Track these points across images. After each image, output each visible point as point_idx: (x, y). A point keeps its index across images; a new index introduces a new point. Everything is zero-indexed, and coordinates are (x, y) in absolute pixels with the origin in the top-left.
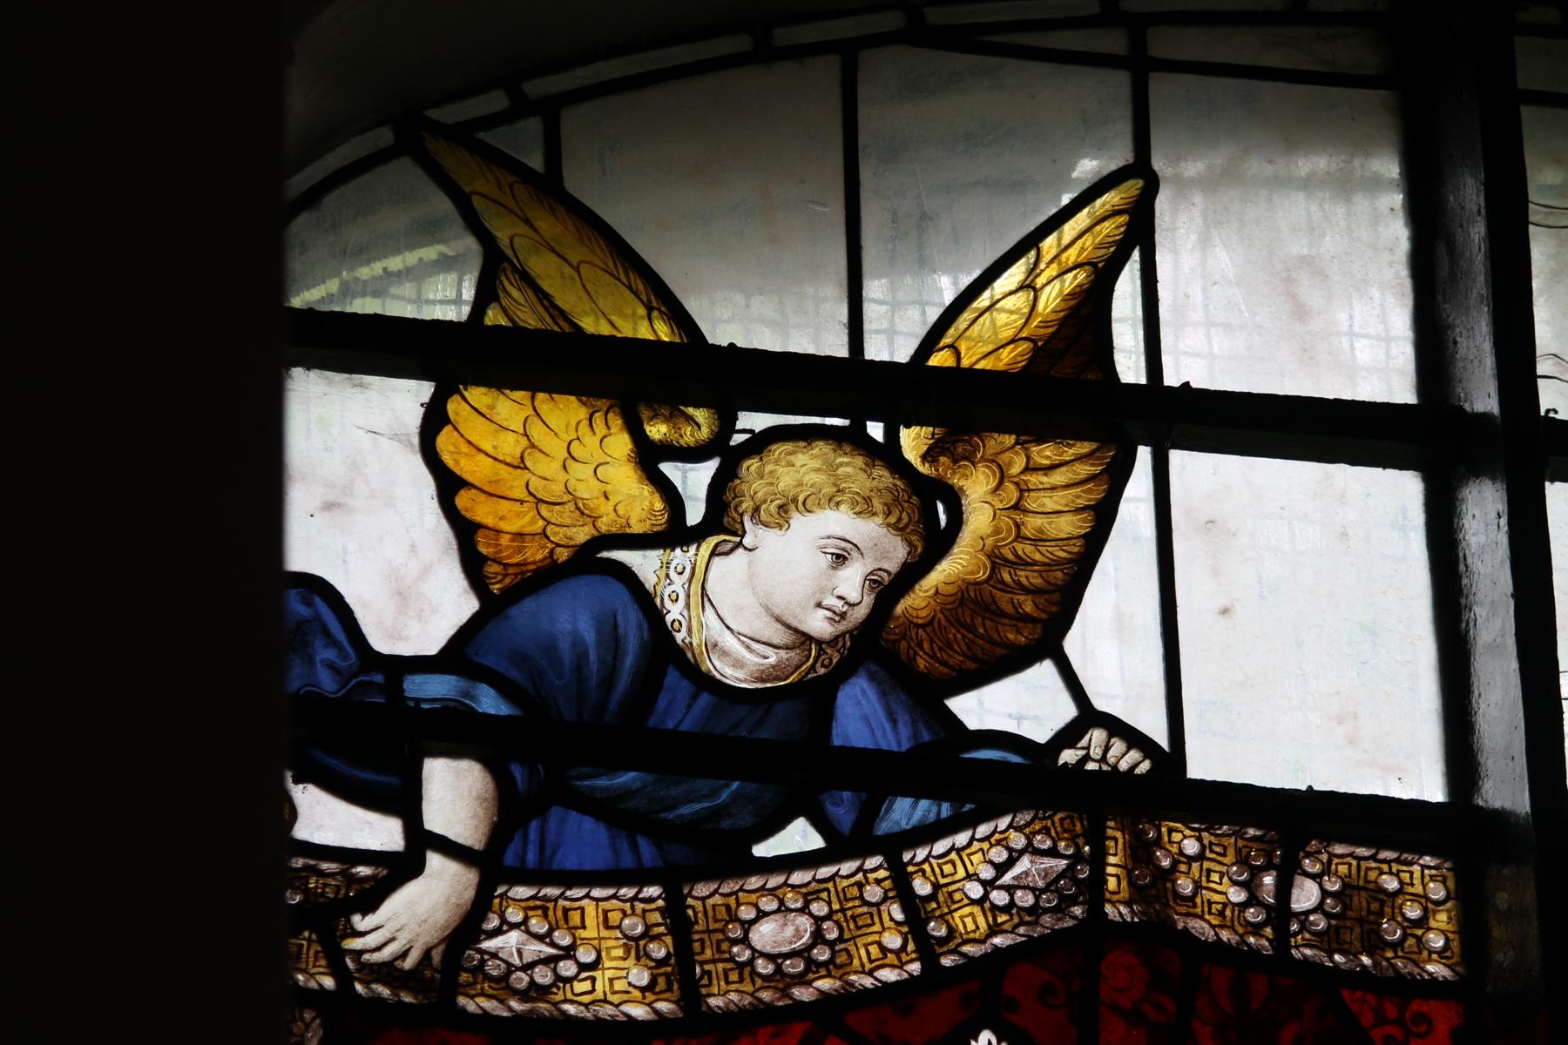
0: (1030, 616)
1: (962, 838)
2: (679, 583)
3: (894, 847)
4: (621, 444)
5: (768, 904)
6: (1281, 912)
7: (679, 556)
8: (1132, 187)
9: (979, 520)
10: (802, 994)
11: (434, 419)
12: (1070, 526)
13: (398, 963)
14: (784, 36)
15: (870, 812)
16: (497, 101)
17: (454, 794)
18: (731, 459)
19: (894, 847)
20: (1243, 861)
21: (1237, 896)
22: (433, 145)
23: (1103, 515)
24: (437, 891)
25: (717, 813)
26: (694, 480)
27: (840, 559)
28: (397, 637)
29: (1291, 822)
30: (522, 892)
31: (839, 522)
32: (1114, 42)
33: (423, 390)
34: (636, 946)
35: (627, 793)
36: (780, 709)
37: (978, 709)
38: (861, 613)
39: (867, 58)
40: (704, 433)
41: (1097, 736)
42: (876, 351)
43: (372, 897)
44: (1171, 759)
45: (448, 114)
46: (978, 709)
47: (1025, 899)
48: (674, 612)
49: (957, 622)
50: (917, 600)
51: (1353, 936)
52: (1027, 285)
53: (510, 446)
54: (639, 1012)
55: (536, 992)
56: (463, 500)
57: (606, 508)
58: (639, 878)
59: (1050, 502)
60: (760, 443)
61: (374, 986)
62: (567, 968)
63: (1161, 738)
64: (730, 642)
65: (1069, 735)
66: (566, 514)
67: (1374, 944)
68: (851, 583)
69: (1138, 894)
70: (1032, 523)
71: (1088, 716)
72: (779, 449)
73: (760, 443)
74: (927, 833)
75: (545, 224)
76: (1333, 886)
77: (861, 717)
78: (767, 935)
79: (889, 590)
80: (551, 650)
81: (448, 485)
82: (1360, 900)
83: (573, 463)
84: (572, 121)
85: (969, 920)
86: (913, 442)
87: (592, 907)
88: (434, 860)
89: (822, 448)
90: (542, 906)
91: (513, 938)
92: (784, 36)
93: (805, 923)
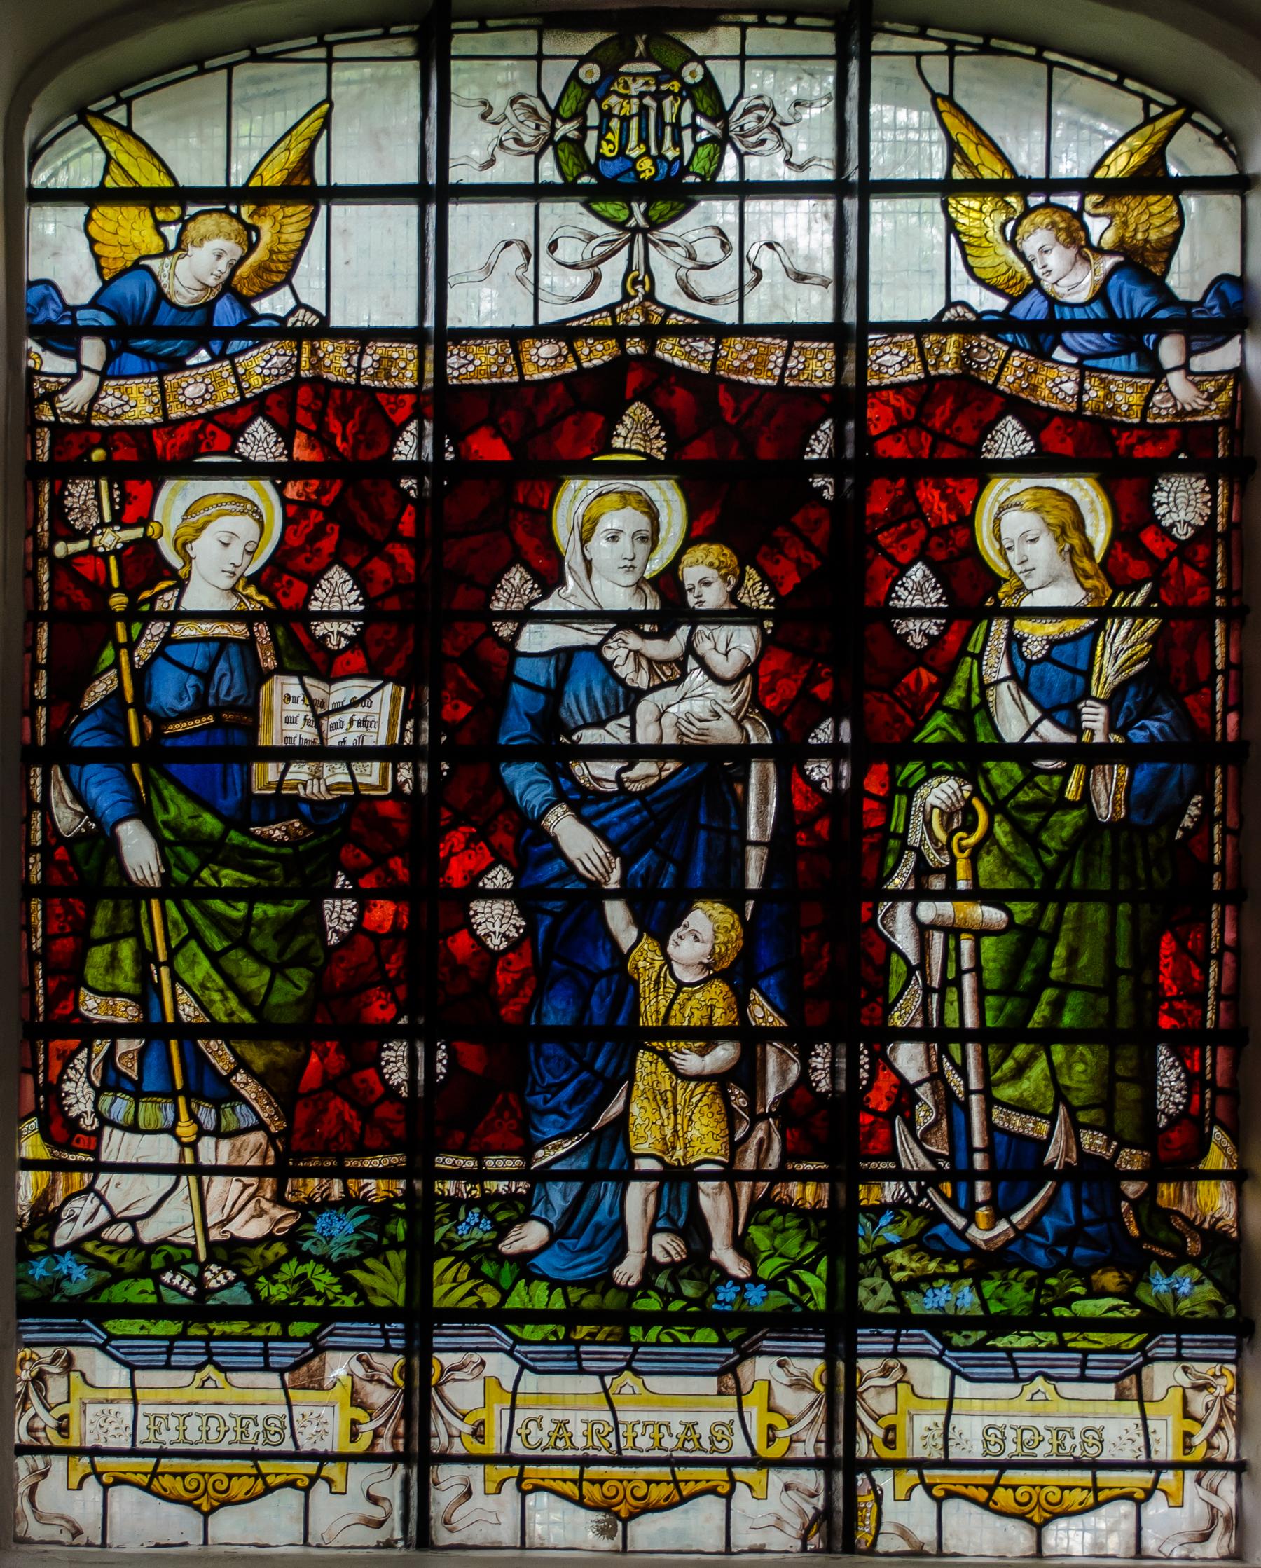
0: (281, 273)
1: (254, 352)
2: (166, 271)
3: (231, 358)
4: (150, 222)
5: (191, 381)
6: (358, 369)
7: (167, 261)
8: (326, 106)
9: (266, 237)
10: (201, 411)
11: (89, 219)
12: (298, 237)
13: (967, 624)
14: (208, 64)
15: (225, 347)
16: (111, 100)
17: (93, 351)
18: (184, 222)
19: (231, 358)
20: (347, 352)
21: (345, 364)
22: (91, 120)
23: (308, 231)
24: (88, 383)
25: (176, 351)
26: (171, 232)
27: (219, 257)
28: (75, 298)
29: (364, 336)
30: (113, 383)
31: (219, 243)
32: (321, 53)
33: (86, 209)
34: (148, 399)
35: (147, 347)
36: (198, 312)
37: (263, 306)
38: (226, 276)
39: (236, 69)
40: (177, 216)
41: (301, 312)
42: (233, 184)
43: (65, 389)
44: (325, 320)
45: (94, 107)
46: (263, 306)
47: (275, 372)
48: (164, 281)
49: (258, 276)
50: (243, 270)
51: (382, 375)
52: (288, 149)
53: (111, 227)
54: (149, 421)
55: (117, 416)
56: (97, 248)
57: (143, 246)
58: (149, 375)
59: (290, 229)
60: (193, 218)
61: (87, 705)
62: (126, 408)
63: (324, 313)
64: (182, 291)
65: (292, 313)
66: (130, 249)
67: (388, 376)
68: (223, 266)
69: (312, 366)
70: (284, 237)
71: (300, 305)
72: (201, 218)
73: (193, 218)
74: (243, 352)
75: (124, 142)
76: (376, 357)
77: (226, 314)
78: (190, 392)
79: (235, 268)
80: (125, 298)
81: (92, 242)
82: (385, 362)
83: (132, 230)
84: (137, 105)
85: (256, 381)
86: (245, 211)
87: (134, 385)
88: (85, 374)
89: (215, 216)
90: (119, 387)
91: (110, 399)
92: (208, 64)
93: (203, 386)
